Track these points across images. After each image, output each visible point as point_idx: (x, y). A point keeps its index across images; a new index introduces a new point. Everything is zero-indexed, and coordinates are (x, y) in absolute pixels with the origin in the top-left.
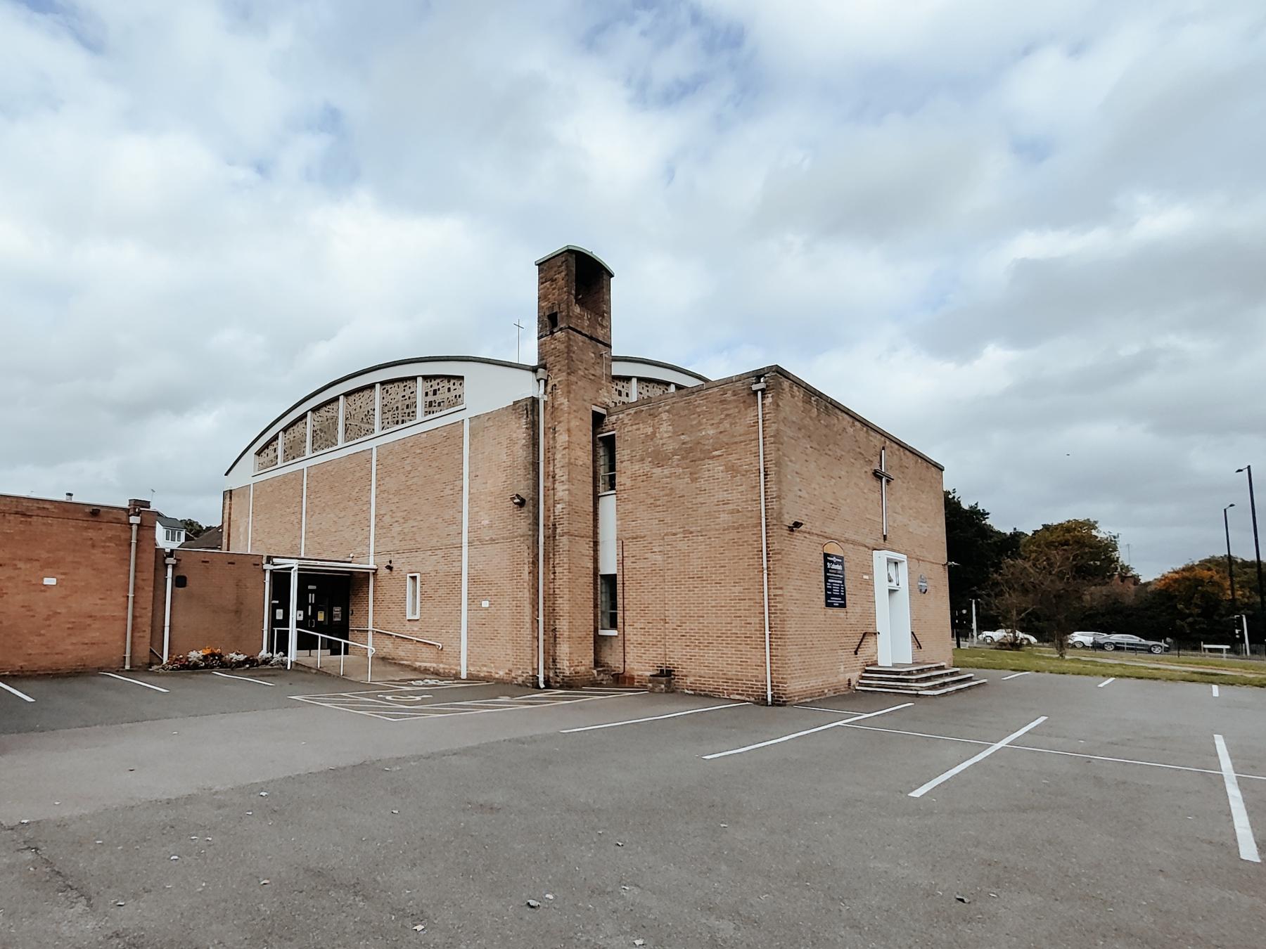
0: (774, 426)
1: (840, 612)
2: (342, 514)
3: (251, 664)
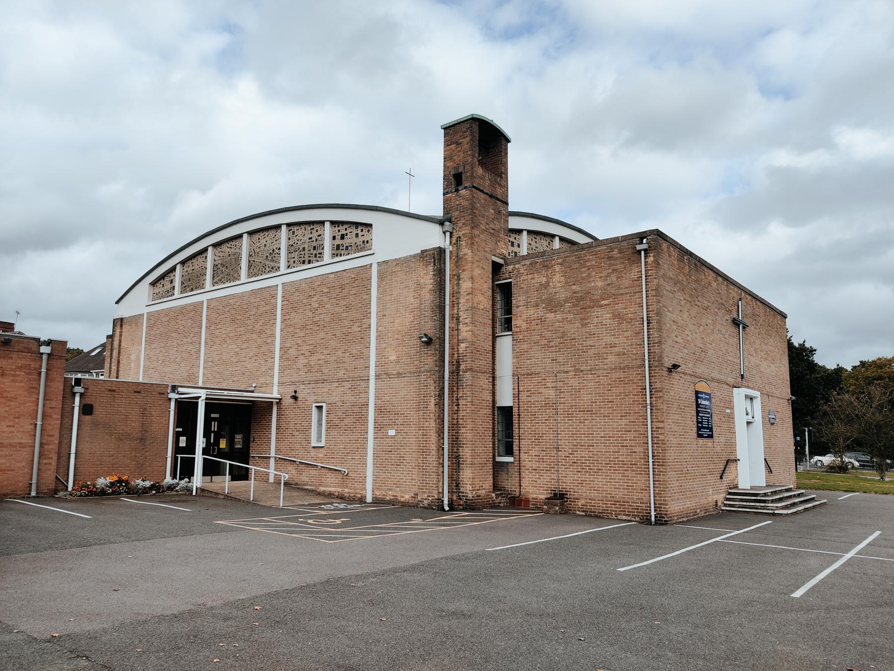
0: (655, 282)
1: (709, 442)
2: (244, 346)
3: (158, 490)
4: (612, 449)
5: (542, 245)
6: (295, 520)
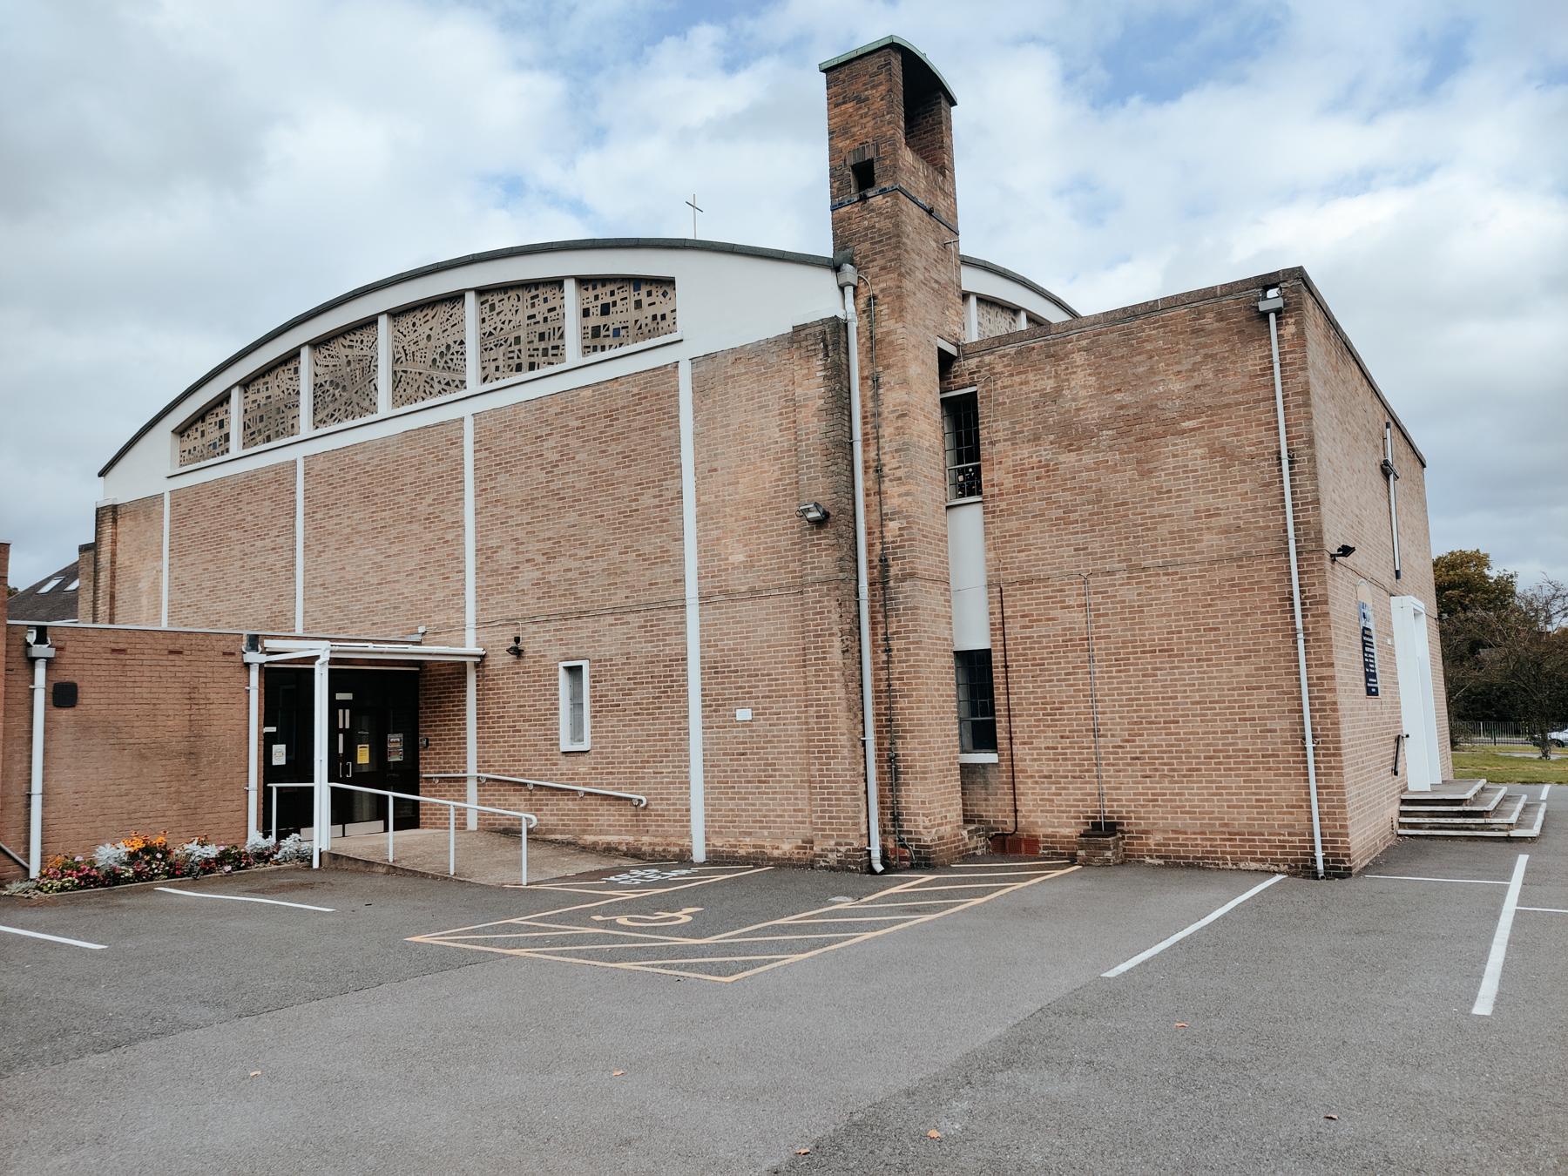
3: (235, 863)
4: (1219, 726)
5: (1000, 325)
6: (583, 918)
